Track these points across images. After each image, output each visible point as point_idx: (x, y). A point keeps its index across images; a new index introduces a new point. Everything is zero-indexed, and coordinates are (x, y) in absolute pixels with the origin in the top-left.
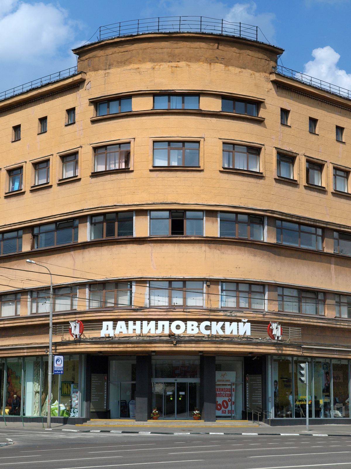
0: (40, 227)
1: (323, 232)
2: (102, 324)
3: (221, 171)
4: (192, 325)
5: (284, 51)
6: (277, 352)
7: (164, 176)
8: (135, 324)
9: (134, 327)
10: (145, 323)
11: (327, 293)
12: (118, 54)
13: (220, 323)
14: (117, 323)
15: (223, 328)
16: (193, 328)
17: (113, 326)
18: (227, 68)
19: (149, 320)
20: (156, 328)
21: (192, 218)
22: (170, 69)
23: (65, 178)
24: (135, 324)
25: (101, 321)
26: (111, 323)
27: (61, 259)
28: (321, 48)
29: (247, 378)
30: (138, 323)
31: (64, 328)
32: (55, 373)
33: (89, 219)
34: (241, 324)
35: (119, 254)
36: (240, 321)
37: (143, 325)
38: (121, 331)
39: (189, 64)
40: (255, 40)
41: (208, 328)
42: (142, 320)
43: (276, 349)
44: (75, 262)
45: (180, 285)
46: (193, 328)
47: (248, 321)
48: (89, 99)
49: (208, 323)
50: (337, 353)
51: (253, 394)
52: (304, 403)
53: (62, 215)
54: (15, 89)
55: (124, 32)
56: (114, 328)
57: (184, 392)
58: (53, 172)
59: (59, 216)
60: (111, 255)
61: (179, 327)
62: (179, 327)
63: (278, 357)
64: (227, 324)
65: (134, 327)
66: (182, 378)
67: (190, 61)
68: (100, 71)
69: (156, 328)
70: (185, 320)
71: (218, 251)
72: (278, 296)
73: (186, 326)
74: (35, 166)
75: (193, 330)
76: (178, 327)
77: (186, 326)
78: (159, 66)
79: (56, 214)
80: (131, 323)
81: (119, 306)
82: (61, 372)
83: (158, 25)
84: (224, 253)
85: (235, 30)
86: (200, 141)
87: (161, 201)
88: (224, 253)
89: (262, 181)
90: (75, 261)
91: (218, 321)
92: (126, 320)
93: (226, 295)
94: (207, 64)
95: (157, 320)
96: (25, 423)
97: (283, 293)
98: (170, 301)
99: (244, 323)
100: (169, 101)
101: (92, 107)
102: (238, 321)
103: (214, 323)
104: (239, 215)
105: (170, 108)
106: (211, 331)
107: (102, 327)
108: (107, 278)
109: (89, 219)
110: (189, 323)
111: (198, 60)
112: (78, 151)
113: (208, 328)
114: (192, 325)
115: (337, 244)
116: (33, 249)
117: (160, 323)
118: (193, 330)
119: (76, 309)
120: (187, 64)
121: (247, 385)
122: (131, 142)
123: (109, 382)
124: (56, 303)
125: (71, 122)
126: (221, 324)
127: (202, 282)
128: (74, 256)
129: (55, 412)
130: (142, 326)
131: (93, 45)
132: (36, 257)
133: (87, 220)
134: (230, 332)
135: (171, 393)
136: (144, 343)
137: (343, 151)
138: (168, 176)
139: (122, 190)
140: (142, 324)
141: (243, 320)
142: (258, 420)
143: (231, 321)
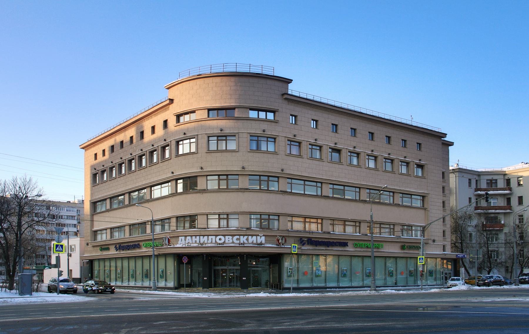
0: (110, 261)
1: (393, 194)
3: (175, 157)
4: (229, 238)
5: (447, 134)
6: (156, 155)
8: (196, 238)
9: (196, 239)
10: (201, 237)
11: (285, 256)
13: (245, 237)
15: (247, 239)
16: (229, 239)
19: (204, 236)
20: (208, 240)
21: (342, 256)
22: (303, 257)
23: (159, 196)
24: (196, 238)
25: (178, 237)
26: (183, 238)
28: (512, 189)
30: (198, 237)
31: (62, 210)
32: (291, 246)
34: (259, 237)
36: (258, 235)
37: (256, 240)
38: (189, 242)
40: (273, 75)
41: (237, 239)
42: (200, 236)
45: (71, 218)
46: (229, 239)
47: (263, 235)
49: (238, 237)
52: (298, 250)
53: (244, 213)
54: (200, 68)
55: (213, 71)
57: (181, 283)
58: (338, 224)
63: (107, 273)
64: (250, 237)
65: (196, 239)
66: (81, 267)
69: (208, 240)
70: (224, 236)
72: (141, 132)
73: (216, 239)
74: (151, 153)
75: (229, 241)
76: (220, 239)
77: (216, 239)
79: (83, 143)
80: (194, 237)
81: (252, 229)
82: (417, 309)
83: (184, 145)
85: (379, 113)
87: (156, 165)
89: (277, 124)
91: (244, 235)
92: (191, 236)
93: (84, 220)
95: (208, 236)
96: (182, 185)
97: (292, 220)
98: (333, 196)
99: (261, 237)
100: (371, 216)
102: (257, 235)
103: (242, 237)
104: (261, 177)
105: (222, 148)
106: (240, 241)
110: (227, 237)
113: (237, 239)
114: (229, 238)
115: (94, 183)
116: (251, 136)
117: (210, 237)
118: (229, 241)
119: (371, 215)
123: (192, 269)
124: (94, 220)
125: (153, 128)
126: (246, 237)
127: (208, 220)
129: (274, 223)
131: (233, 300)
132: (133, 122)
134: (145, 133)
135: (345, 269)
136: (378, 297)
137: (511, 236)
140: (200, 238)
141: (260, 235)
142: (148, 277)
143: (252, 236)
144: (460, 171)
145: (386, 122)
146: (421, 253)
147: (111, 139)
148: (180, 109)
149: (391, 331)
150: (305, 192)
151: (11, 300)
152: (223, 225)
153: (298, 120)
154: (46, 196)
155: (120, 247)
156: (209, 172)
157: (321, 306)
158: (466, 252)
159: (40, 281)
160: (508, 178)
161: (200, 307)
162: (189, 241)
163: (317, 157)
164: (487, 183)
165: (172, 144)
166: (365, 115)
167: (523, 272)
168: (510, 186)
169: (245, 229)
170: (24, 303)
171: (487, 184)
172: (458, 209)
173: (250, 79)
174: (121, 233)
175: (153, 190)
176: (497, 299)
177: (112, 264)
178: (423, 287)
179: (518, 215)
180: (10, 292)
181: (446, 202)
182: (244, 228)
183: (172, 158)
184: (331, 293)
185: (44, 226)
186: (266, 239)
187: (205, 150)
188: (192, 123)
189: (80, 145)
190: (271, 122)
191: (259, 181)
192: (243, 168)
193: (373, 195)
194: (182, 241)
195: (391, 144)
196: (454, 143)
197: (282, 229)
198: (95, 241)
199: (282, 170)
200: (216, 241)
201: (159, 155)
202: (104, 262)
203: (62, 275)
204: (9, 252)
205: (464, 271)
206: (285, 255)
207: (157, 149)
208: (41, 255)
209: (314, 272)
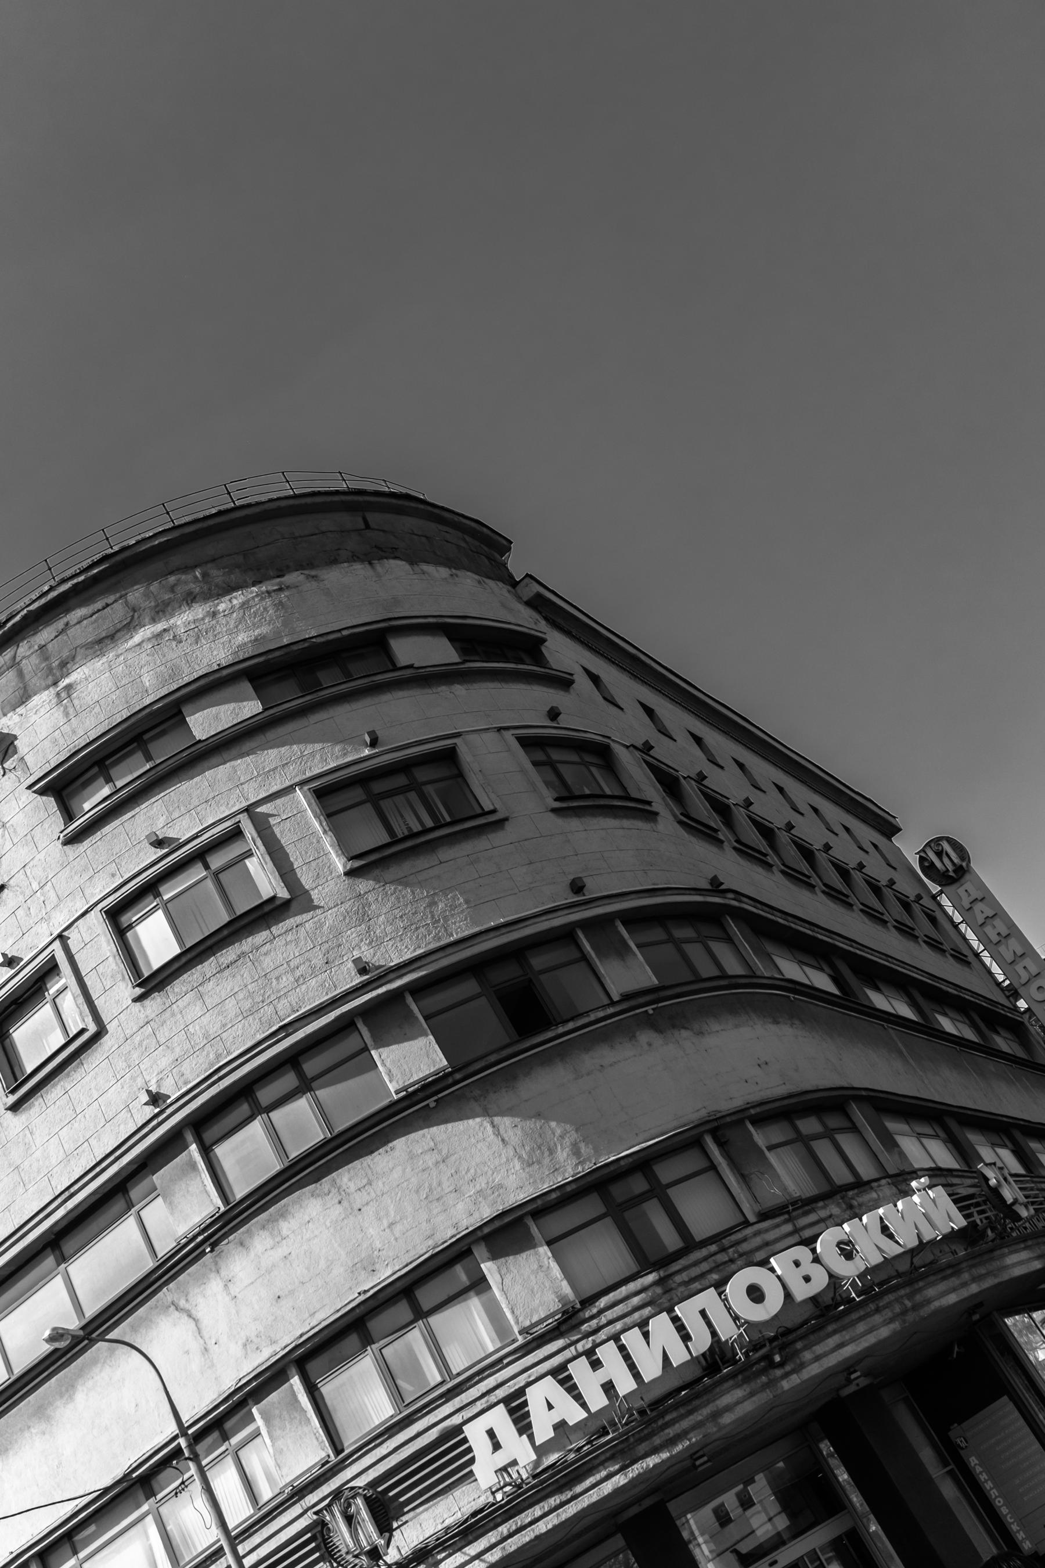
2: (465, 1440)
3: (554, 810)
4: (797, 1264)
7: (403, 875)
9: (602, 1376)
12: (78, 626)
14: (526, 1401)
17: (515, 1422)
18: (416, 568)
24: (596, 1365)
27: (151, 1321)
29: (958, 1441)
33: (189, 1136)
35: (370, 1183)
39: (313, 573)
43: (1032, 1255)
44: (196, 1321)
48: (29, 787)
50: (705, 1542)
51: (1017, 1482)
56: (522, 1423)
59: (72, 1190)
60: (340, 1202)
61: (758, 1293)
62: (758, 1293)
65: (602, 1376)
67: (311, 565)
68: (35, 697)
71: (685, 1033)
73: (729, 1309)
76: (999, 1502)
77: (729, 1309)
78: (229, 603)
84: (702, 1033)
86: (454, 748)
88: (702, 1033)
90: (194, 1319)
94: (362, 566)
101: (50, 802)
107: (470, 1450)
108: (365, 1292)
109: (189, 1136)
111: (333, 561)
112: (53, 955)
118: (807, 1279)
120: (309, 575)
121: (973, 1464)
122: (243, 825)
128: (182, 1303)
130: (627, 1357)
133: (184, 1140)
138: (414, 871)
139: (277, 978)
144: (292, 1385)
145: (16, 1301)
146: (34, 1148)
147: (711, 946)
148: (341, 1301)
149: (198, 624)
150: (433, 1384)
151: (478, 1188)
152: (401, 832)
153: (684, 1382)
154: (453, 1158)
155: (880, 1284)
156: (915, 970)
157: (1031, 1401)
158: (39, 1161)
159: (576, 1143)
160: (314, 577)
161: (242, 1220)
162: (555, 1417)
163: (483, 1346)
164: (814, 1549)
165: (74, 951)
166: (572, 608)
167: (16, 674)
168: (397, 836)
169: (134, 919)
170: (1039, 1405)
171: (330, 815)
172: (546, 1125)
173: (489, 836)
174: (373, 1393)
175: (671, 939)
176: (926, 1037)
177: (746, 1403)
178: (532, 886)
179: (88, 1030)
180: (760, 1332)
181: (1015, 963)
182: (966, 946)
183: (106, 1019)
184: (141, 549)
185: (323, 1536)
186: (751, 1297)
187: (127, 991)
188: (181, 896)
189: (892, 870)
190: (592, 1010)
191: (689, 1357)
192: (155, 1099)
193: (95, 867)
194: (497, 1446)
195: (706, 878)
196: (564, 1419)
197: (271, 1117)
198: (16, 1081)
199: (577, 887)
200: (736, 1318)
201: (500, 1380)
202: (779, 1513)
203: (520, 1434)
204: (295, 746)
205: (943, 1027)
206: (206, 856)
207: (731, 1549)
208: (1037, 1018)
209: (547, 1153)
